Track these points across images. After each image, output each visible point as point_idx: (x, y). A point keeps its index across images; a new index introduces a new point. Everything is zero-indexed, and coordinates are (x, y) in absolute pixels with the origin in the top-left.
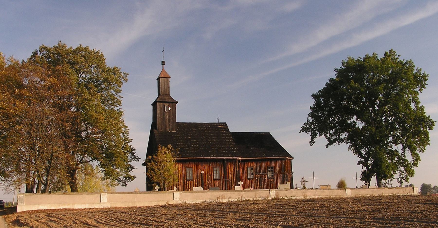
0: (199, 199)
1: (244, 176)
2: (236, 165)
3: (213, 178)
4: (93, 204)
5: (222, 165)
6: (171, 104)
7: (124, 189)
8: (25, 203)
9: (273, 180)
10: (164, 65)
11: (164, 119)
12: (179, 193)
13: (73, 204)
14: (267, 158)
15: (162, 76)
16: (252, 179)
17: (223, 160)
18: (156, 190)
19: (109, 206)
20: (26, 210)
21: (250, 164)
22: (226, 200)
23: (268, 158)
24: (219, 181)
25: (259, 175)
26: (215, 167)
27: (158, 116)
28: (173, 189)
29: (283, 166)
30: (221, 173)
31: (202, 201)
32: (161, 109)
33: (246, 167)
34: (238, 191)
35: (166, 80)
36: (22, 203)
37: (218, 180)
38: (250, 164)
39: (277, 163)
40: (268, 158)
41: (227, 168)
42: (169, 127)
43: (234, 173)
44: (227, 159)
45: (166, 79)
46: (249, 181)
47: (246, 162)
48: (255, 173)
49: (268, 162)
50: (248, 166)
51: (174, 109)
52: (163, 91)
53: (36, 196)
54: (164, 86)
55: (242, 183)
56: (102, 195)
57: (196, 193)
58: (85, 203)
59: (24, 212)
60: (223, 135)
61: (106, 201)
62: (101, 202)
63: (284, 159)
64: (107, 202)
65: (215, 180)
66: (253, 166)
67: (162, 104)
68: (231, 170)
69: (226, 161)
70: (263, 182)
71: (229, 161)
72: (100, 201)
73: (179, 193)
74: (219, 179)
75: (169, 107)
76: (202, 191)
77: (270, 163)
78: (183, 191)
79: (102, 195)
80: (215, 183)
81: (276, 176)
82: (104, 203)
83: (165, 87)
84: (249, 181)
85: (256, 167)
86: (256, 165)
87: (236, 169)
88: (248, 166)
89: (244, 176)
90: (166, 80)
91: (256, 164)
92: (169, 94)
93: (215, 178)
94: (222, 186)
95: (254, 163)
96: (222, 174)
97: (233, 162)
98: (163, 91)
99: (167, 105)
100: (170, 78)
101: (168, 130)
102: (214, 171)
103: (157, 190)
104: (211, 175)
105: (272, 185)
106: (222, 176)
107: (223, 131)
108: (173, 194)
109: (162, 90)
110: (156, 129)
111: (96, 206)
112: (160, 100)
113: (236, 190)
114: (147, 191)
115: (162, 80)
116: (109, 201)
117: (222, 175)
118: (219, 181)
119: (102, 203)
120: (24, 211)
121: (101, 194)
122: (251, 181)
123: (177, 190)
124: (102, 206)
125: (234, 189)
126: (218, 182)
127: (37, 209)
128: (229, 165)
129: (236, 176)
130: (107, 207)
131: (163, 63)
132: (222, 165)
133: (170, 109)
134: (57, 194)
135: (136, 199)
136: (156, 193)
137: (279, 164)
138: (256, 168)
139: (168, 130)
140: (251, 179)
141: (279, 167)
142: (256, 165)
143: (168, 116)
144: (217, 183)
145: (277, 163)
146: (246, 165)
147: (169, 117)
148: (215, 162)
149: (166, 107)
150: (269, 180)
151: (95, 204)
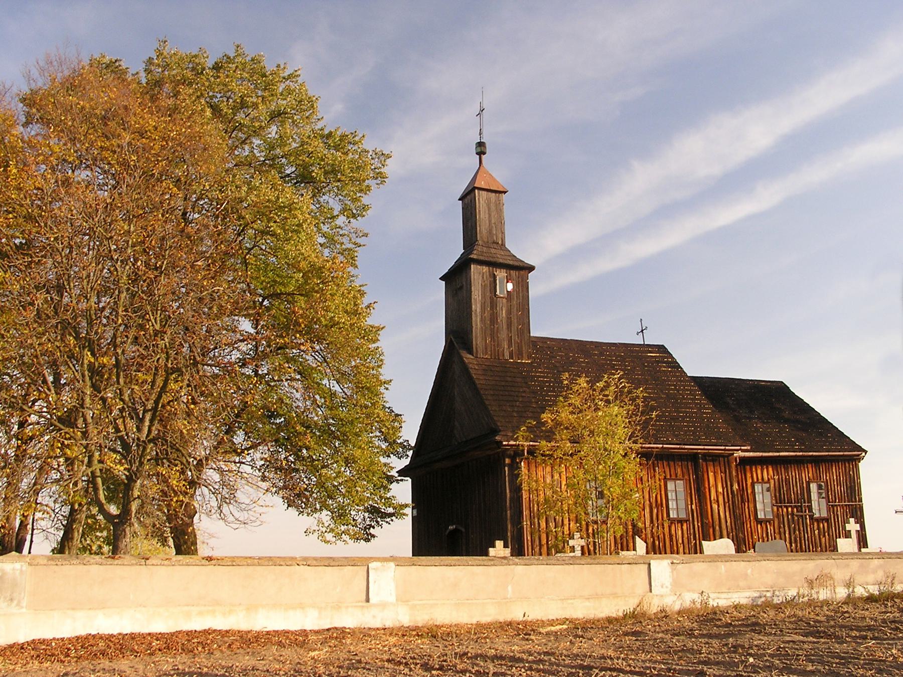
0: (739, 589)
1: (747, 510)
2: (730, 473)
3: (665, 515)
4: (338, 606)
5: (691, 471)
6: (513, 273)
7: (360, 549)
8: (24, 604)
9: (826, 525)
10: (484, 153)
11: (494, 318)
12: (669, 561)
13: (251, 608)
14: (811, 454)
15: (482, 185)
16: (769, 521)
17: (693, 458)
18: (573, 549)
19: (404, 617)
20: (29, 639)
21: (759, 472)
22: (842, 593)
23: (814, 454)
24: (685, 527)
25: (787, 507)
26: (670, 479)
27: (473, 307)
28: (634, 549)
29: (850, 483)
30: (689, 499)
31: (748, 594)
32: (484, 287)
33: (749, 481)
34: (717, 558)
35: (493, 200)
36: (12, 600)
37: (681, 521)
38: (759, 472)
39: (834, 470)
40: (814, 454)
41: (707, 486)
42: (510, 345)
43: (726, 500)
44: (704, 455)
45: (494, 194)
46: (759, 526)
47: (748, 467)
48: (777, 503)
49: (810, 466)
50: (755, 480)
51: (523, 287)
52: (484, 232)
53: (81, 567)
54: (487, 216)
55: (583, 542)
56: (375, 569)
57: (728, 563)
58: (302, 606)
59: (22, 647)
60: (670, 381)
61: (392, 599)
62: (368, 600)
63: (849, 461)
64: (395, 600)
65: (672, 521)
66: (768, 479)
67: (485, 269)
68: (717, 491)
69: (702, 459)
70: (800, 533)
71: (710, 461)
72: (364, 597)
73: (669, 561)
74: (686, 521)
75: (507, 282)
76: (731, 556)
77: (816, 470)
78: (677, 556)
79: (375, 569)
80: (673, 532)
81: (833, 513)
82: (383, 605)
83: (490, 221)
84: (759, 526)
85: (777, 484)
86: (776, 477)
87: (732, 486)
88: (755, 480)
89: (747, 510)
90: (493, 200)
91: (778, 474)
92: (503, 244)
93: (671, 516)
94: (695, 543)
95: (770, 469)
96: (692, 504)
97: (722, 463)
98: (484, 232)
99: (501, 274)
100: (505, 192)
101: (507, 356)
102: (669, 494)
103: (578, 553)
104: (659, 505)
105: (823, 540)
106: (692, 510)
107: (664, 367)
108: (647, 566)
109: (482, 229)
110: (469, 348)
111: (349, 620)
112: (482, 258)
113: (709, 556)
114: (413, 556)
115: (481, 199)
116: (402, 599)
117: (694, 507)
118: (685, 527)
119: (375, 605)
120: (22, 640)
121: (370, 565)
122: (767, 529)
123: (647, 553)
124: (374, 617)
125: (701, 552)
126: (682, 529)
127: (83, 632)
128: (711, 474)
129: (733, 509)
130: (398, 625)
131: (481, 149)
132: (691, 471)
133: (510, 287)
134: (659, 559)
135: (510, 588)
136: (573, 562)
137: (838, 476)
138: (777, 489)
139: (507, 356)
140: (767, 521)
141: (839, 484)
142: (776, 477)
143: (506, 312)
144: (680, 532)
145: (834, 470)
146: (749, 475)
147: (509, 312)
148: (672, 463)
149: (498, 281)
150: (816, 524)
151: (347, 607)
